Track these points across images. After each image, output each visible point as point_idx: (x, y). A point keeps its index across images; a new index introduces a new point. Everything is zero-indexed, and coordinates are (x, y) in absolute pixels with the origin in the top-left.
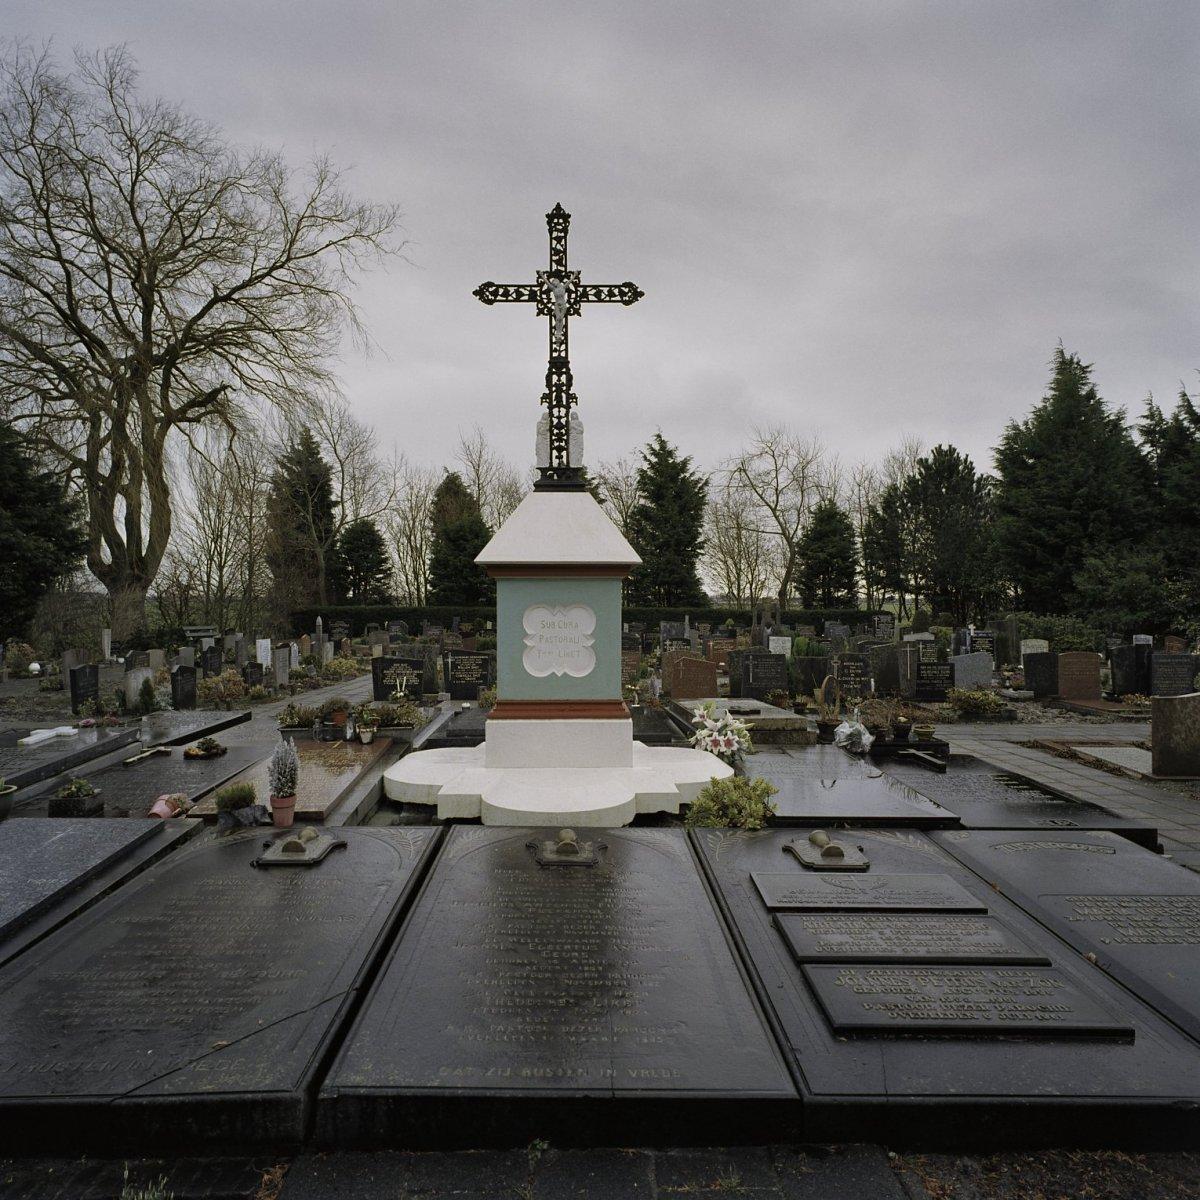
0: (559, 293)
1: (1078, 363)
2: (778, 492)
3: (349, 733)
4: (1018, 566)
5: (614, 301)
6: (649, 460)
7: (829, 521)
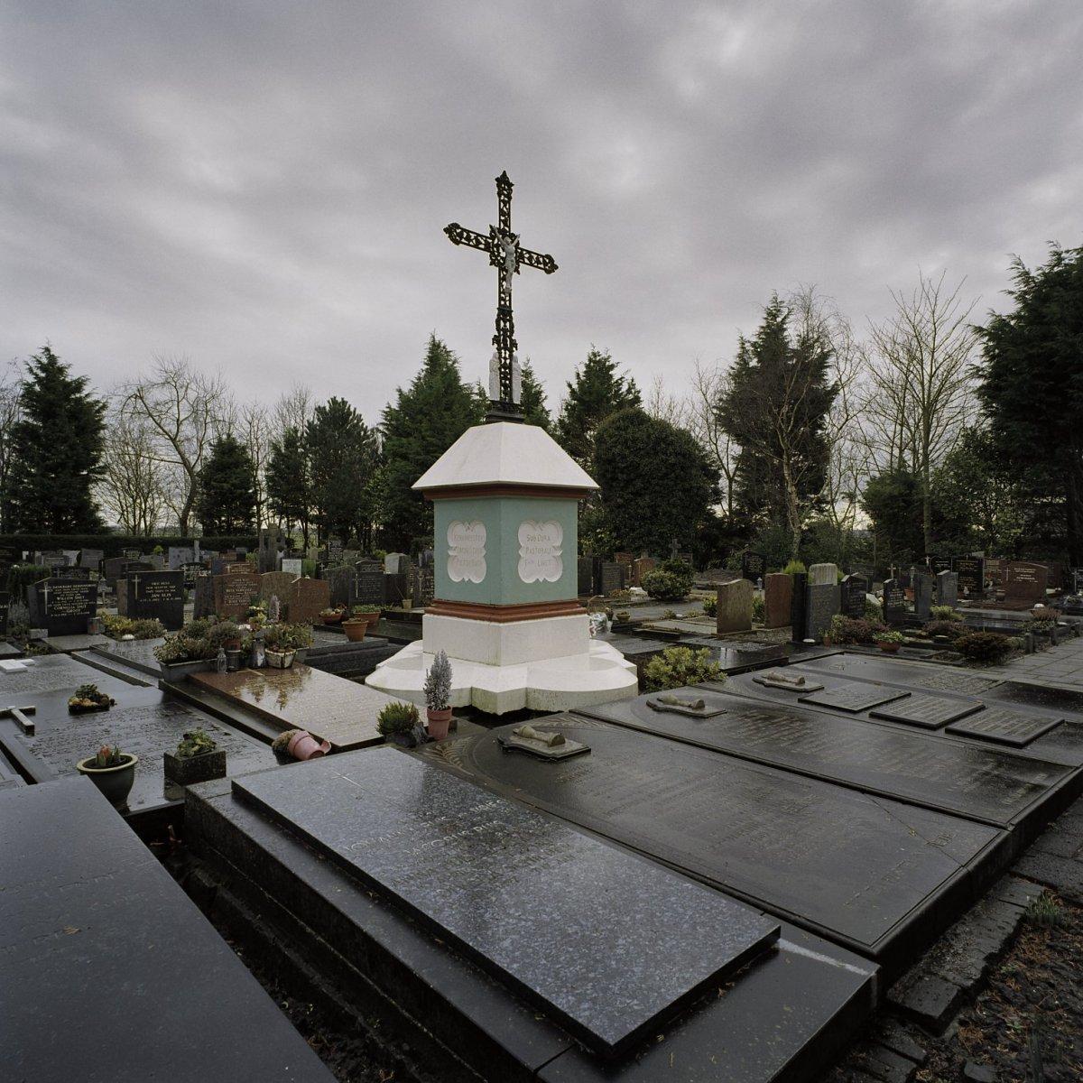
0: (502, 249)
1: (444, 347)
2: (179, 423)
3: (260, 660)
4: (410, 501)
5: (540, 268)
6: (36, 375)
7: (229, 458)
